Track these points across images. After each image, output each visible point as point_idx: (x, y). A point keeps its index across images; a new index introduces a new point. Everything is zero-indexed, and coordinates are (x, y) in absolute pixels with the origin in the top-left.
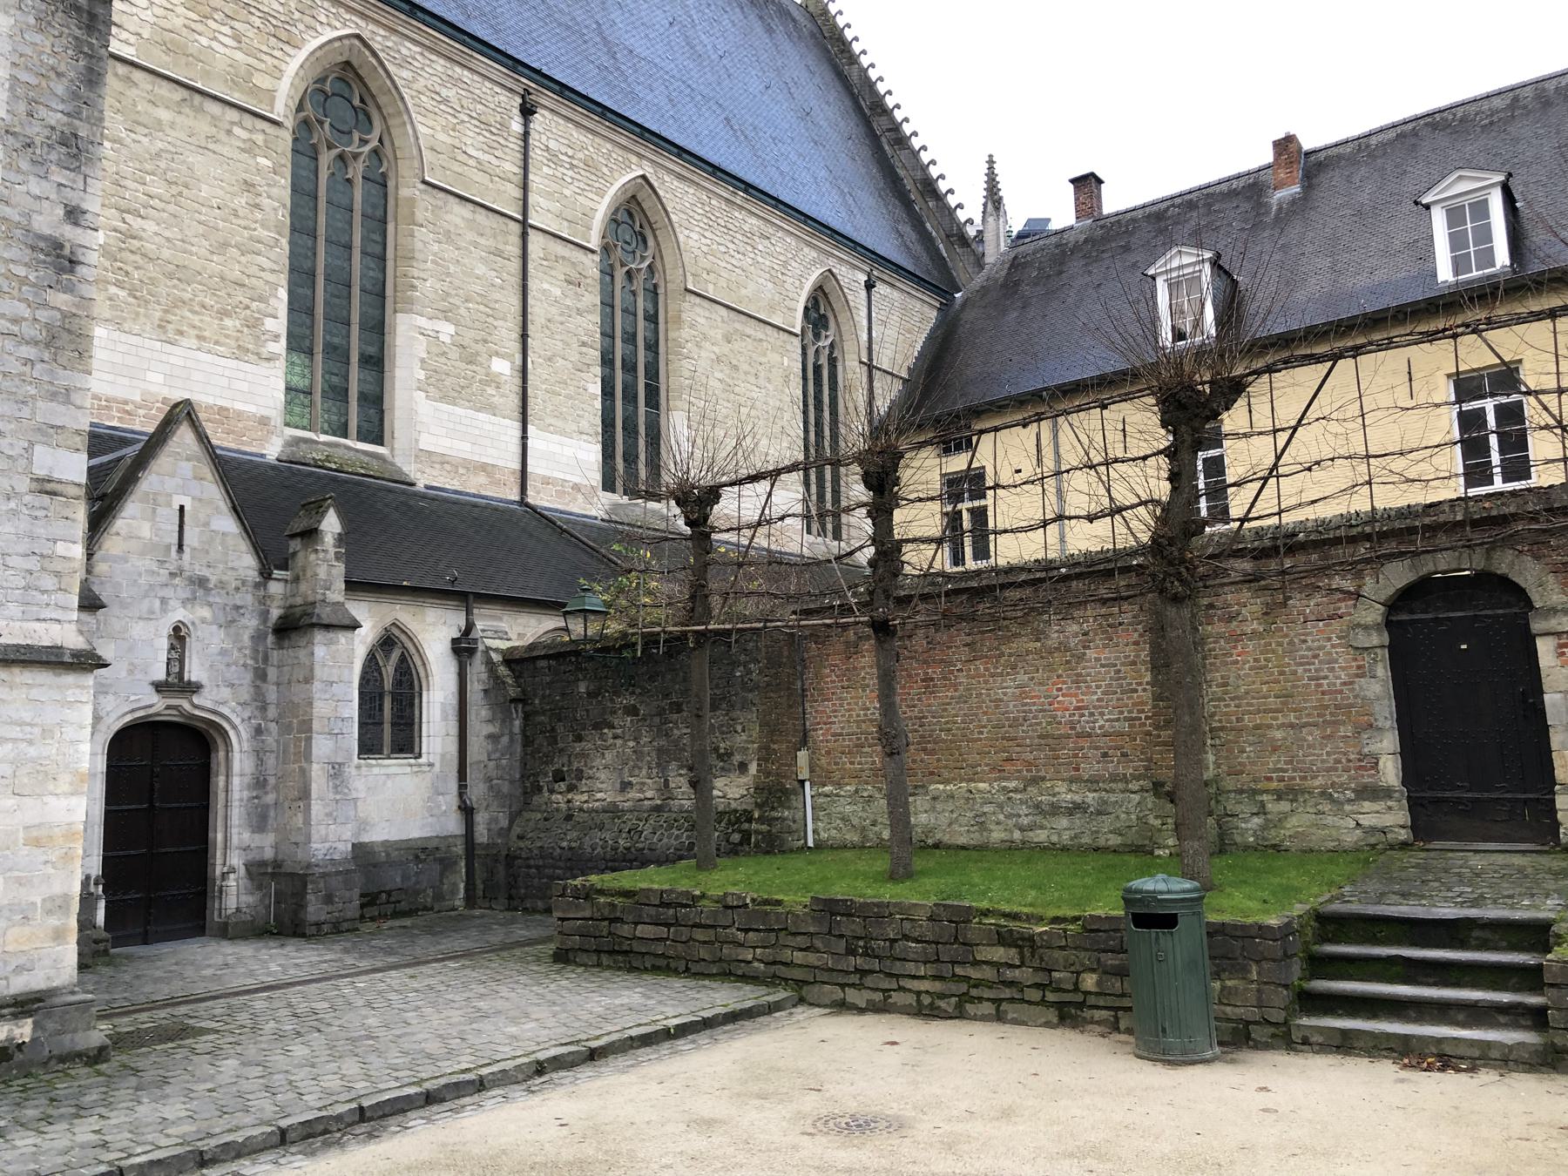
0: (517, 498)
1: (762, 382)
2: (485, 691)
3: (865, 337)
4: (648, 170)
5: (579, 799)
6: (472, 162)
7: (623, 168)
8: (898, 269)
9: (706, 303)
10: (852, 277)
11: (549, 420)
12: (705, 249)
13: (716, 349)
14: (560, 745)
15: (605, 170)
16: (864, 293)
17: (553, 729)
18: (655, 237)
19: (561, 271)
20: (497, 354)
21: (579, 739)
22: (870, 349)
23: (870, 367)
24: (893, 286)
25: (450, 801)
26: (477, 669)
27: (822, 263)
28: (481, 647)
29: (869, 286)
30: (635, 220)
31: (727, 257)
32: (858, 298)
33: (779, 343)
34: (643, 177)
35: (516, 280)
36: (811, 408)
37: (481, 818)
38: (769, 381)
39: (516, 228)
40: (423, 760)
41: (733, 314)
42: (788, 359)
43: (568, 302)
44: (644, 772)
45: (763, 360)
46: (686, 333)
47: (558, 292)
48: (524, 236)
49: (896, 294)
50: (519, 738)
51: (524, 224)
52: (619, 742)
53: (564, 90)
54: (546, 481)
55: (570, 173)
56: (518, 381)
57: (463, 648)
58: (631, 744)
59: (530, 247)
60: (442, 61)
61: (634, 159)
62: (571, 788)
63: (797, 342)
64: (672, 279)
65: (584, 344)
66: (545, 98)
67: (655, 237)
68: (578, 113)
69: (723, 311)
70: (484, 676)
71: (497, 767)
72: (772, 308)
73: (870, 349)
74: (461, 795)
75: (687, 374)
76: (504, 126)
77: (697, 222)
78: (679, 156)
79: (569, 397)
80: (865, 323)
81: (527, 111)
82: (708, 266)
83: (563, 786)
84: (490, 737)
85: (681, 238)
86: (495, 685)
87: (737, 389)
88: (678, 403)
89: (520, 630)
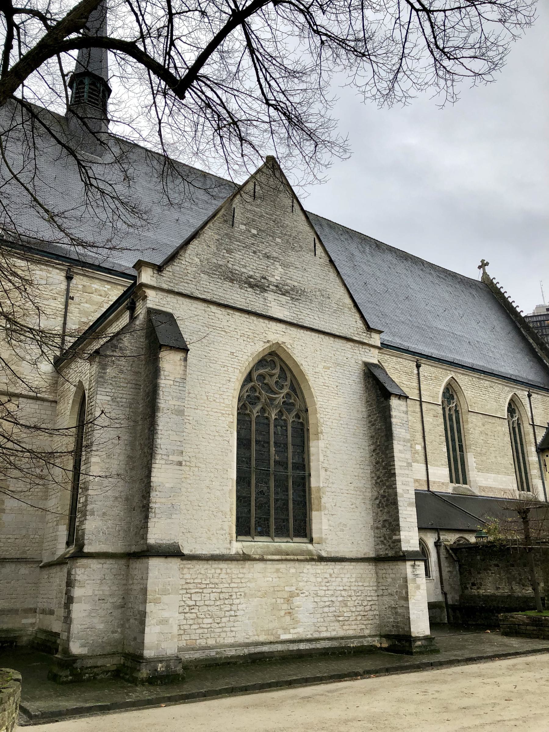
0: (427, 489)
1: (496, 438)
2: (446, 558)
3: (530, 415)
4: (453, 375)
5: (482, 592)
6: (405, 386)
7: (445, 376)
8: (539, 388)
9: (475, 414)
10: (523, 394)
11: (433, 462)
12: (473, 396)
13: (480, 429)
14: (473, 575)
15: (441, 378)
16: (527, 399)
17: (470, 570)
18: (457, 395)
19: (432, 413)
20: (417, 444)
21: (479, 573)
22: (532, 419)
23: (533, 425)
24: (537, 394)
25: (439, 591)
26: (442, 551)
27: (511, 391)
28: (443, 544)
29: (529, 396)
30: (450, 393)
31: (480, 397)
32: (526, 401)
33: (501, 423)
34: (452, 377)
35: (419, 419)
36: (514, 443)
37: (449, 596)
38: (498, 437)
39: (418, 403)
40: (431, 578)
41: (484, 416)
42: (504, 428)
43: (435, 423)
44: (504, 584)
45: (495, 430)
46: (470, 425)
47: (431, 420)
48: (421, 405)
49: (539, 396)
50: (458, 572)
51: (421, 401)
52: (493, 575)
53: (428, 357)
54: (434, 482)
55: (431, 382)
56: (423, 451)
57: (437, 545)
58: (498, 575)
59: (423, 408)
60: (395, 358)
61: (449, 372)
62: (478, 588)
63: (506, 421)
64: (464, 408)
65: (440, 436)
66: (423, 361)
67: (457, 395)
68: (432, 362)
69: (481, 416)
70: (445, 553)
71: (453, 581)
72: (496, 411)
73: (532, 419)
74: (442, 589)
75: (472, 439)
76: (412, 372)
77: (472, 390)
78: (462, 368)
79: (438, 454)
80: (529, 409)
81: (418, 366)
82: (475, 401)
83: (475, 587)
84: (449, 571)
85: (465, 394)
86: (449, 557)
87: (488, 442)
88: (470, 450)
89: (451, 538)
